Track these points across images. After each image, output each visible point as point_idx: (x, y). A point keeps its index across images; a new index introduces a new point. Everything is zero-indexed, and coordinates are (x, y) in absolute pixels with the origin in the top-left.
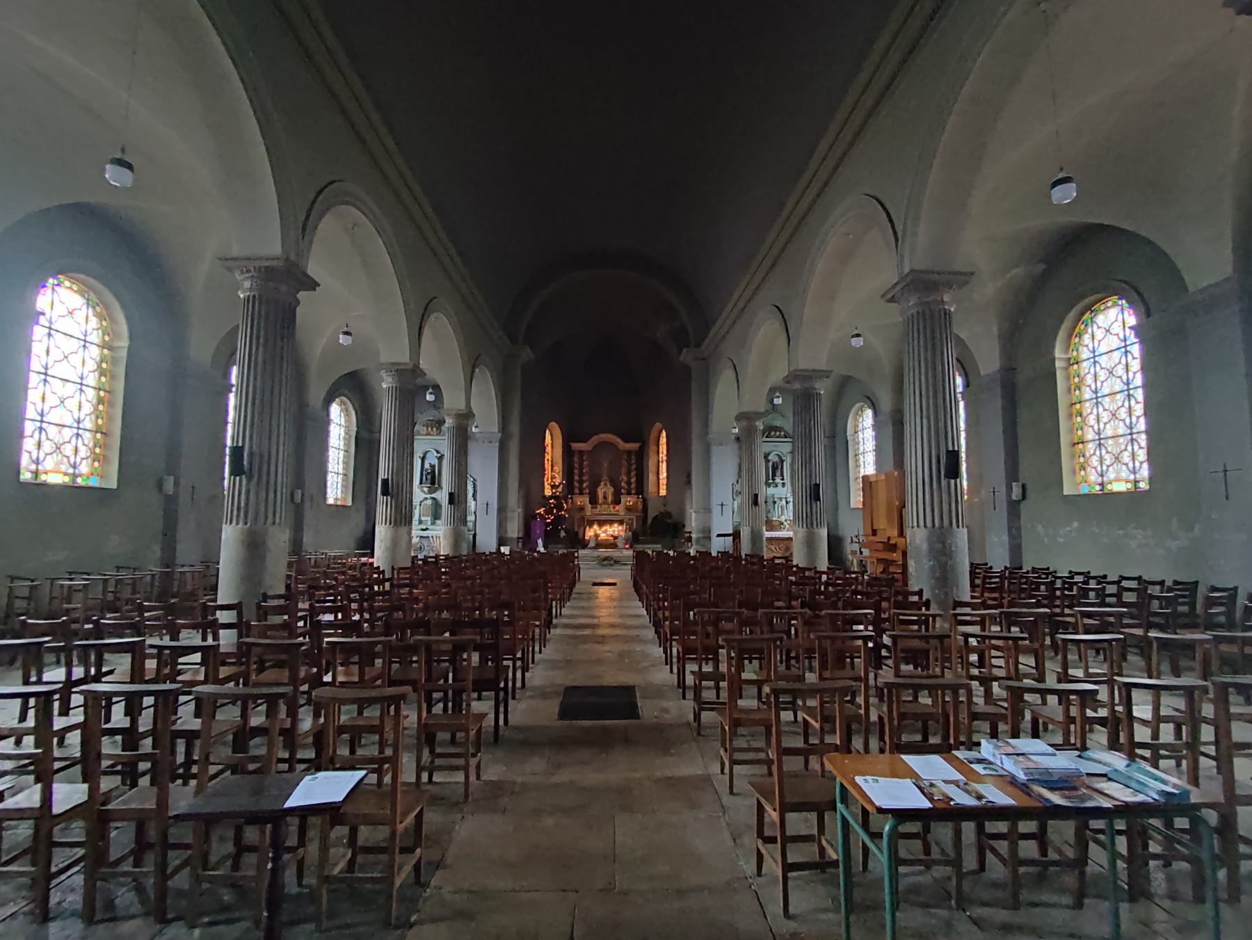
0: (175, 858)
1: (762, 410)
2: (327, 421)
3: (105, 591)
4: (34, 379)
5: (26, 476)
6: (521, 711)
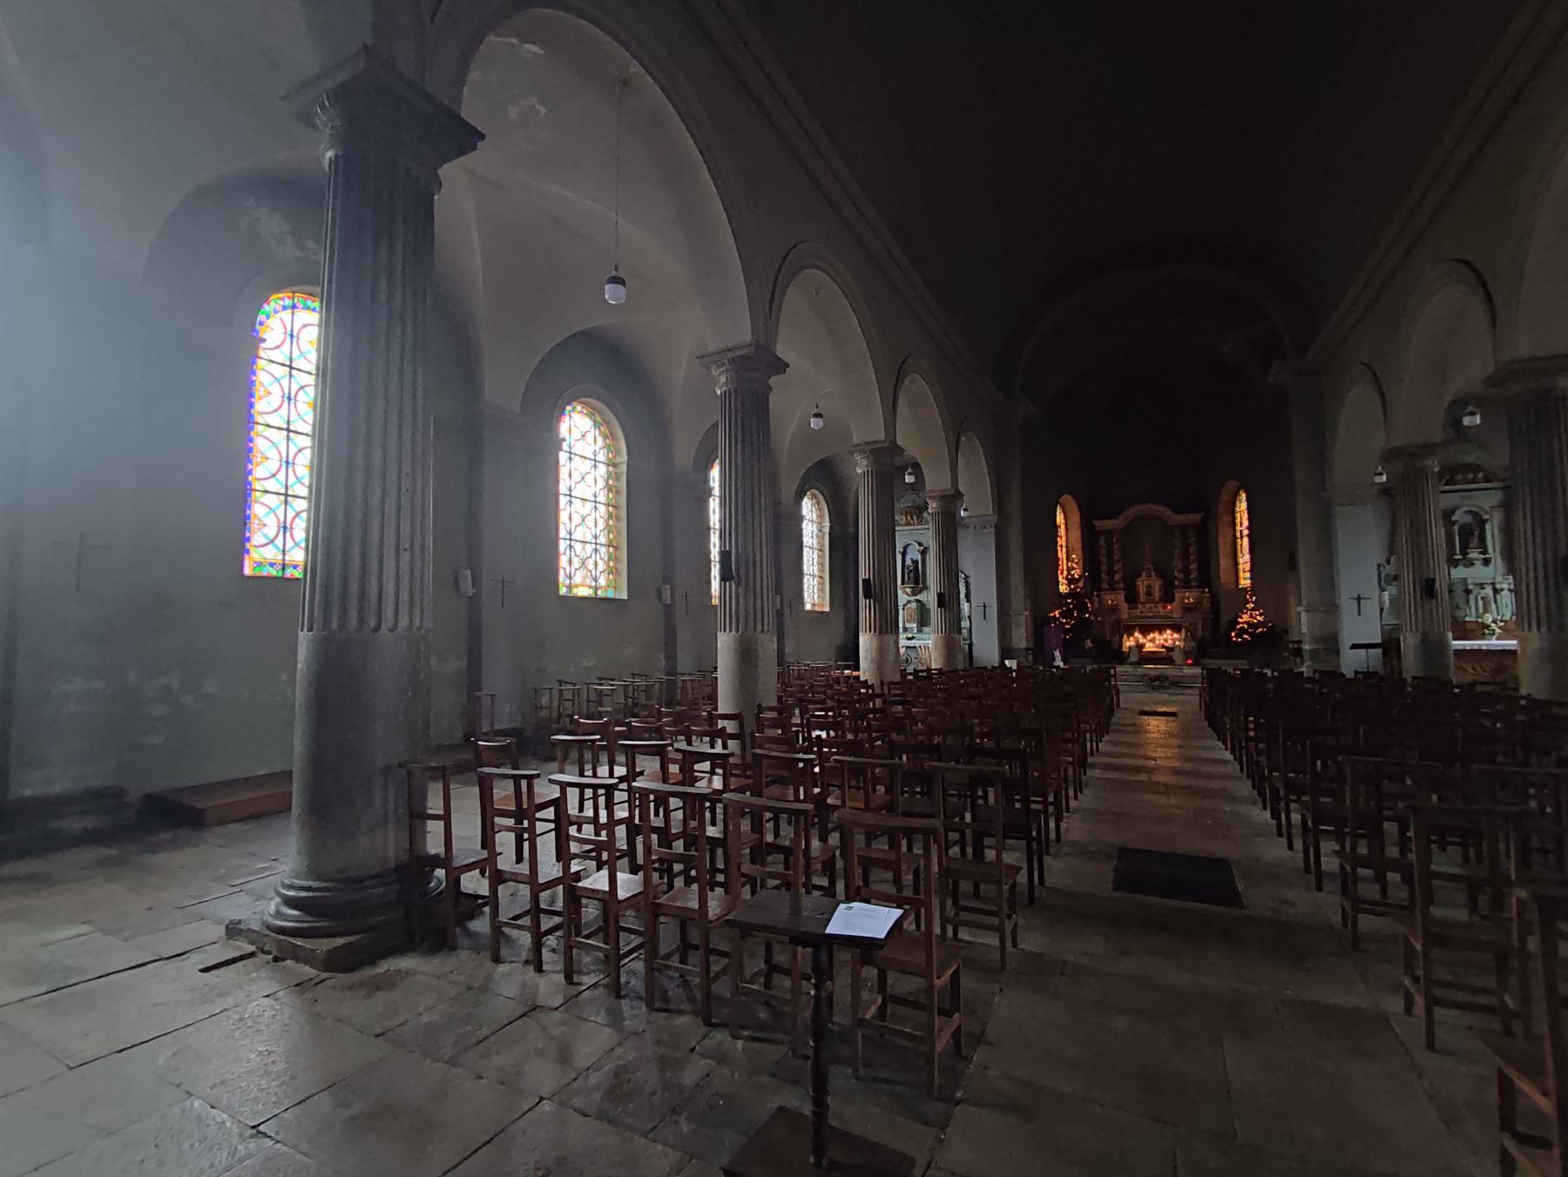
0: (717, 965)
1: (1438, 440)
2: (800, 519)
3: (626, 698)
4: (563, 500)
5: (563, 591)
6: (1057, 870)
